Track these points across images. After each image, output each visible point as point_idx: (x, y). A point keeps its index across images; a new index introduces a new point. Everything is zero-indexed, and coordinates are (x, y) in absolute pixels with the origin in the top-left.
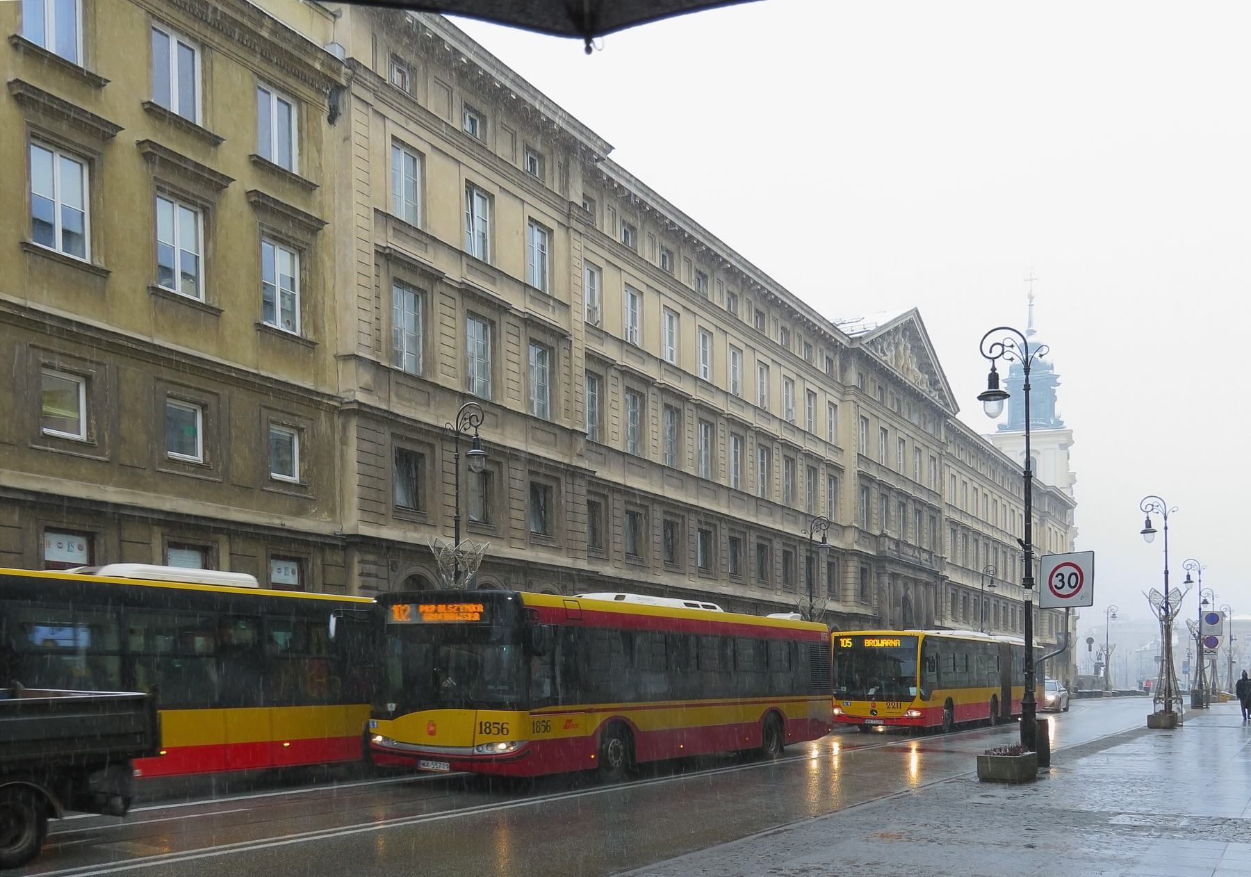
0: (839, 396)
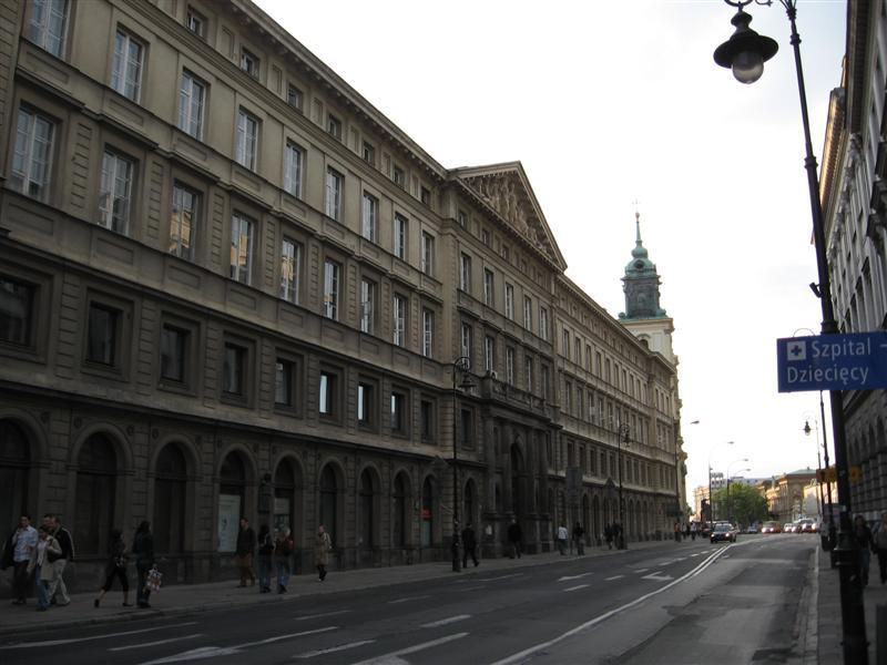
0: (438, 229)
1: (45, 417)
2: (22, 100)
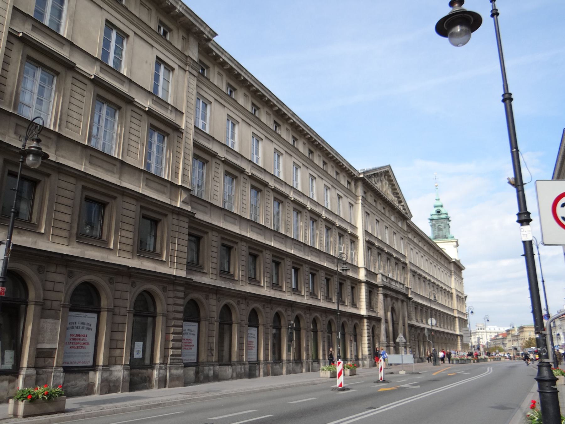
1: (207, 298)
2: (28, 56)
